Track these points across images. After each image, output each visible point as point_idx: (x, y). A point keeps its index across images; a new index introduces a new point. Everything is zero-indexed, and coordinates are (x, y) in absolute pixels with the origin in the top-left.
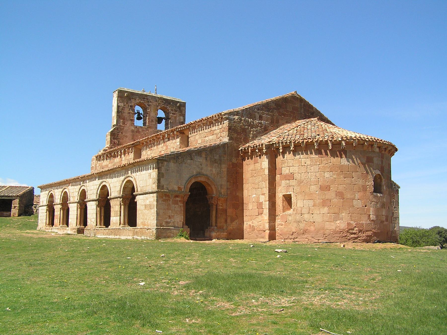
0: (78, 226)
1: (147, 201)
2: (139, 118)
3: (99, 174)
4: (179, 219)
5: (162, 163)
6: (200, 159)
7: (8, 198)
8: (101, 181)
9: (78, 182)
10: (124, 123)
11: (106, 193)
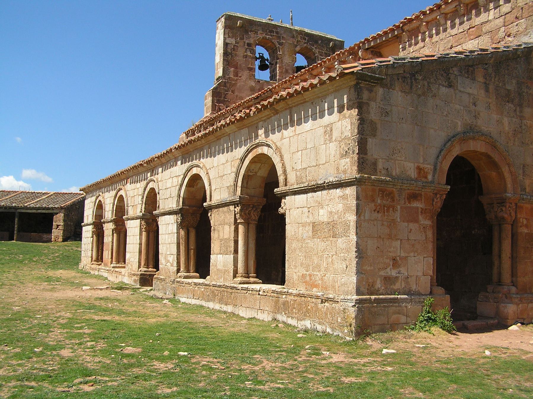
0: (143, 269)
1: (322, 212)
2: (263, 67)
3: (183, 149)
4: (420, 267)
5: (371, 91)
6: (472, 88)
7: (47, 212)
8: (187, 165)
9: (141, 173)
10: (236, 75)
11: (200, 196)
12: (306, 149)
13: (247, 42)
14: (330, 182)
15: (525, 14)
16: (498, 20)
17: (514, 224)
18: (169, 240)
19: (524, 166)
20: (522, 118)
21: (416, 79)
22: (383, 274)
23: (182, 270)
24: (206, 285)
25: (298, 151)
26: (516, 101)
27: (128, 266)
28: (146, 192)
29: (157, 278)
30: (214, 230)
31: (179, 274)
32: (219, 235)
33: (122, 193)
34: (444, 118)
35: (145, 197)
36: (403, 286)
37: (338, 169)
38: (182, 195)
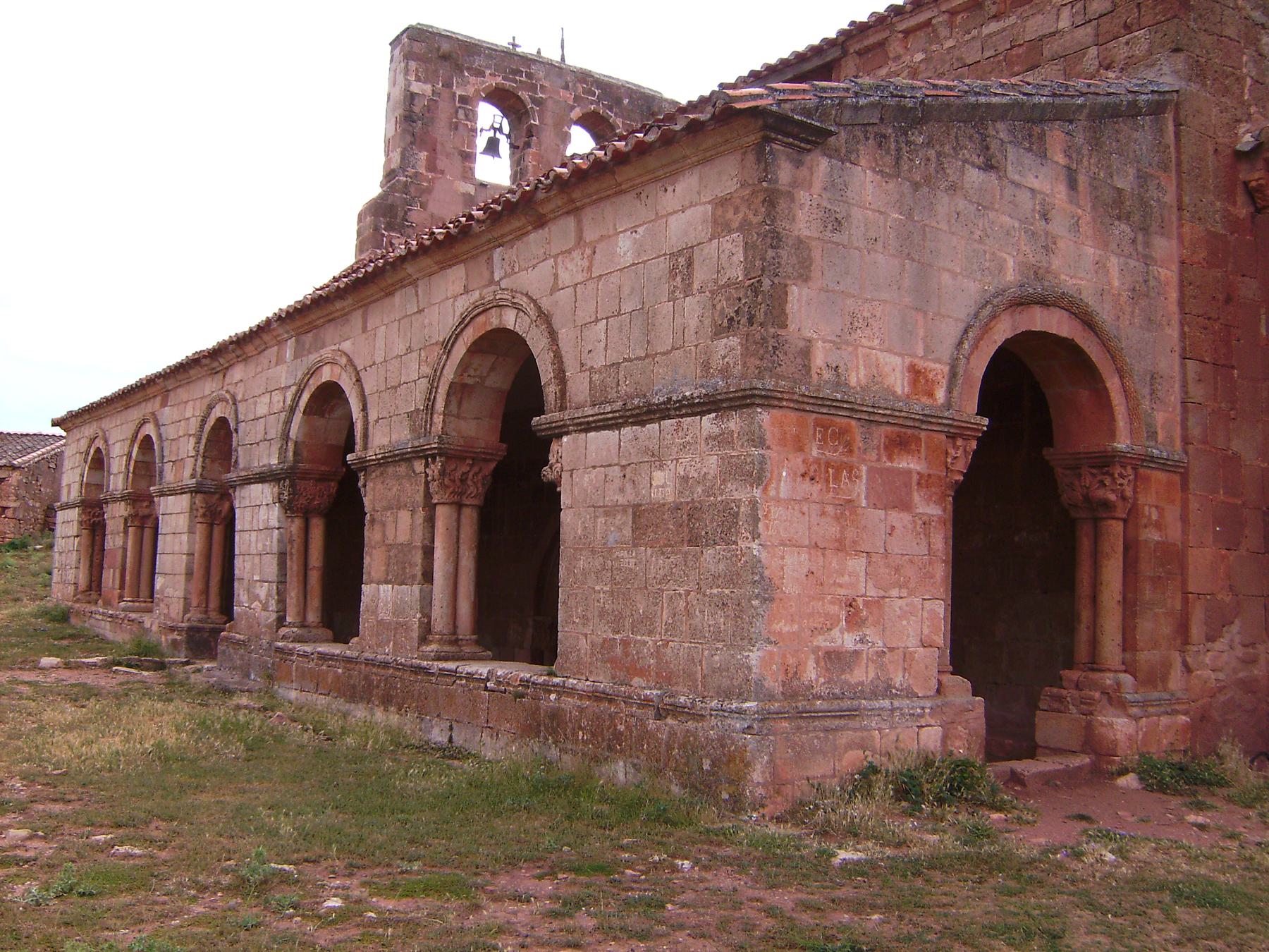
1: (659, 477)
10: (431, 166)
12: (619, 314)
13: (458, 93)
14: (684, 397)
15: (1147, 19)
16: (1081, 31)
17: (1132, 518)
18: (260, 546)
19: (1152, 378)
20: (1147, 260)
21: (908, 143)
22: (823, 644)
23: (289, 619)
24: (349, 660)
25: (597, 321)
26: (1136, 218)
27: (160, 609)
28: (208, 428)
29: (226, 639)
30: (373, 521)
31: (283, 631)
32: (384, 535)
33: (149, 429)
34: (976, 246)
35: (204, 441)
36: (871, 675)
37: (706, 366)
38: (293, 434)
